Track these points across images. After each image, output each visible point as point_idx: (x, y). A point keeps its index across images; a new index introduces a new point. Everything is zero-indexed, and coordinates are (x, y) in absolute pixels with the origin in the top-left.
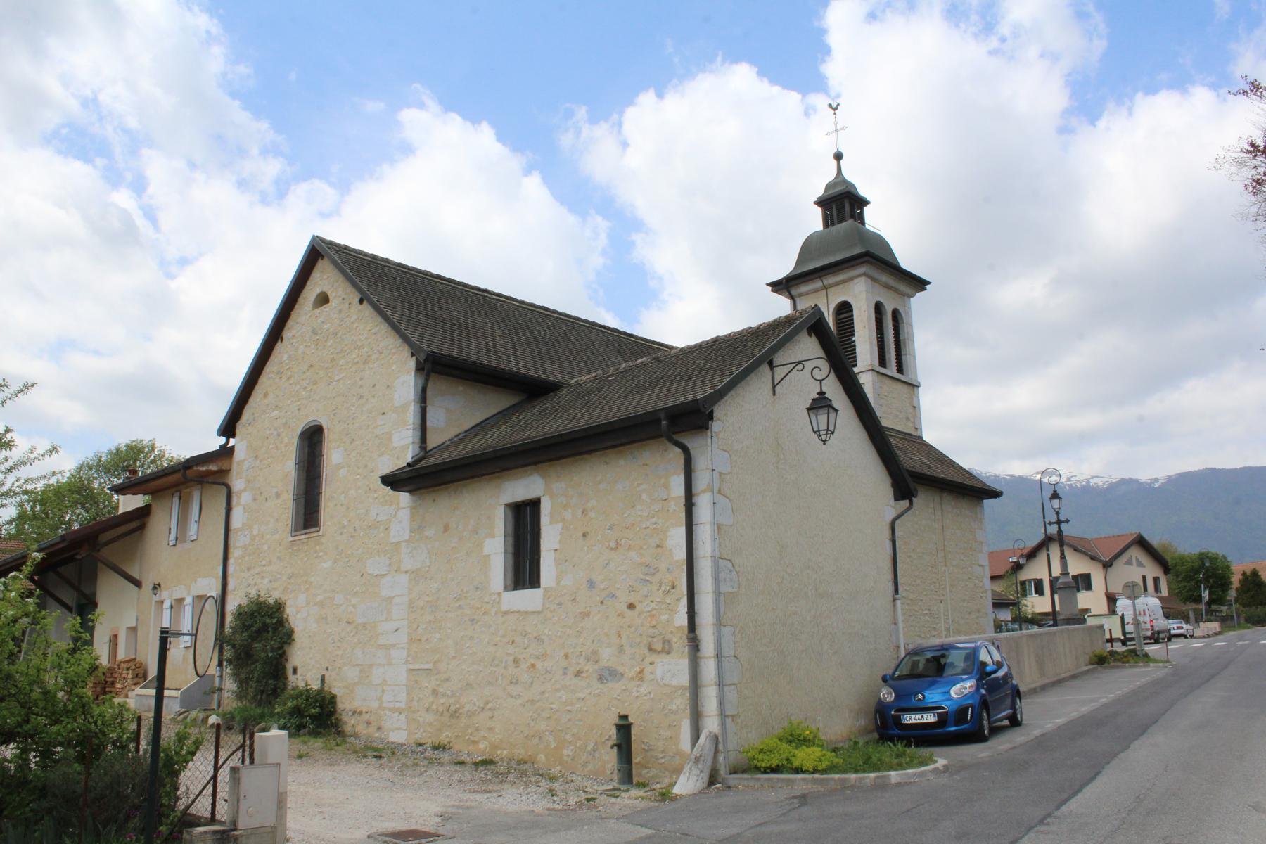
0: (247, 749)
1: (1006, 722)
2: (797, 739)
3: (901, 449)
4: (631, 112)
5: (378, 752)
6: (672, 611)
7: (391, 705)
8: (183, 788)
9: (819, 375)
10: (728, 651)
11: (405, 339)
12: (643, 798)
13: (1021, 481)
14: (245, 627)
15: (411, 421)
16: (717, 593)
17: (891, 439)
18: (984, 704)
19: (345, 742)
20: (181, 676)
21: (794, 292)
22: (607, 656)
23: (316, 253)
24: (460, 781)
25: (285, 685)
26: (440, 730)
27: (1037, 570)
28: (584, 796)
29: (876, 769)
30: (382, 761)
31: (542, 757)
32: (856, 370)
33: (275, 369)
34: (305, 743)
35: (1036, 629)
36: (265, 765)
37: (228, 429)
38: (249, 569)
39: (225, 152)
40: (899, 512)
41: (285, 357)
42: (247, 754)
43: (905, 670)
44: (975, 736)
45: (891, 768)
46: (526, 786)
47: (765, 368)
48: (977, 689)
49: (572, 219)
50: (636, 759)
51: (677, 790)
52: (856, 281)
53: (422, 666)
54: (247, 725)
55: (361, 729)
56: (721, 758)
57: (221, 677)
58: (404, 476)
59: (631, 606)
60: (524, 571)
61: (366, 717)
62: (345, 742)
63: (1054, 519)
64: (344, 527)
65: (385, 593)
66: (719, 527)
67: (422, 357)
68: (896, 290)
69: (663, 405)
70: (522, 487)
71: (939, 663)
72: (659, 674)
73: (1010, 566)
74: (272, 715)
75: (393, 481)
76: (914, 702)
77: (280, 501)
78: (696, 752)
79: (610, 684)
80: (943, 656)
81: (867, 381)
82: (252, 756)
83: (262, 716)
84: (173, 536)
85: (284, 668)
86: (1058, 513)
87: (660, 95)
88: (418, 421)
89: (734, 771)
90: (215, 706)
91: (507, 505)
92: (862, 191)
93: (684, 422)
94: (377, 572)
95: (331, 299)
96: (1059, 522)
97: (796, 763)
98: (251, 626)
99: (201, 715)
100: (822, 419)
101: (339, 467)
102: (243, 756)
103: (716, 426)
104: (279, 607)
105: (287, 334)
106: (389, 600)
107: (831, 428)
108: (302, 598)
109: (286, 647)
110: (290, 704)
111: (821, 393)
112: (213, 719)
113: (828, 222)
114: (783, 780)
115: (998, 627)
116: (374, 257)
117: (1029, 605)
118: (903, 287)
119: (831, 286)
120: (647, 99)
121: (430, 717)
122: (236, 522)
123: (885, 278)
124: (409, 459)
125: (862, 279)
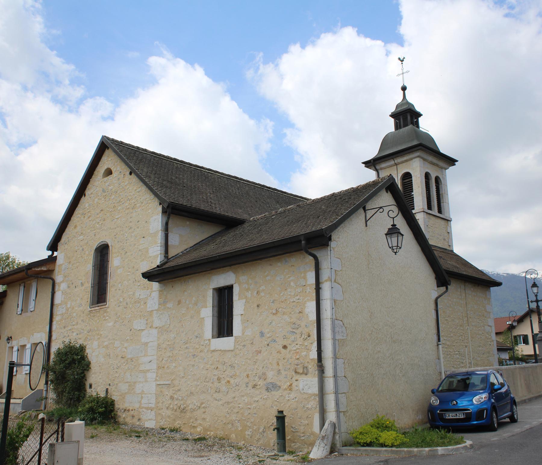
0: (60, 433)
1: (508, 420)
2: (382, 426)
3: (441, 257)
4: (286, 58)
5: (138, 434)
6: (309, 350)
7: (146, 406)
8: (20, 457)
9: (392, 214)
10: (340, 373)
11: (156, 195)
12: (292, 461)
13: (513, 277)
14: (62, 361)
15: (159, 242)
16: (334, 339)
17: (435, 252)
18: (494, 408)
19: (119, 428)
20: (22, 389)
21: (378, 167)
22: (271, 376)
23: (105, 145)
24: (186, 450)
25: (85, 395)
26: (174, 420)
27: (524, 330)
28: (258, 459)
29: (429, 446)
30: (141, 439)
31: (233, 436)
32: (414, 211)
33: (81, 212)
34: (96, 429)
35: (524, 364)
36: (70, 442)
37: (53, 246)
38: (64, 327)
39: (45, 82)
40: (440, 294)
41: (87, 205)
42: (60, 436)
43: (445, 386)
44: (489, 428)
45: (438, 445)
46: (224, 454)
47: (361, 211)
48: (489, 399)
49: (252, 122)
50: (288, 437)
51: (312, 456)
52: (414, 160)
53: (165, 383)
54: (60, 419)
55: (129, 420)
56: (337, 437)
57: (47, 390)
58: (155, 273)
59: (285, 347)
60: (224, 326)
61: (132, 413)
62: (119, 428)
63: (534, 299)
64: (121, 302)
65: (144, 340)
66: (335, 301)
67: (166, 206)
68: (437, 165)
69: (303, 232)
70: (222, 279)
71: (465, 383)
72: (301, 387)
73: (506, 327)
74: (77, 413)
75: (149, 276)
76: (450, 406)
77: (83, 287)
78: (323, 433)
79: (273, 393)
80: (468, 379)
81: (420, 218)
82: (62, 437)
83: (71, 414)
84: (20, 309)
85: (85, 384)
86: (536, 296)
87: (303, 47)
88: (163, 242)
89: (345, 444)
90: (43, 408)
91: (213, 289)
92: (418, 109)
93: (316, 242)
94: (139, 328)
95: (113, 172)
96: (537, 301)
97: (381, 441)
98: (66, 360)
99: (34, 414)
100: (394, 240)
101: (118, 268)
102: (57, 437)
103: (333, 244)
104: (82, 349)
105: (87, 192)
106: (146, 344)
107: (399, 245)
108: (96, 343)
109: (85, 372)
110: (87, 406)
111: (394, 225)
112: (41, 416)
113: (397, 127)
114: (374, 451)
115: (501, 363)
116: (138, 148)
117: (520, 350)
118: (441, 164)
119: (399, 164)
120: (295, 49)
121: (169, 412)
122: (57, 301)
123: (431, 158)
124: (158, 264)
125: (418, 159)
